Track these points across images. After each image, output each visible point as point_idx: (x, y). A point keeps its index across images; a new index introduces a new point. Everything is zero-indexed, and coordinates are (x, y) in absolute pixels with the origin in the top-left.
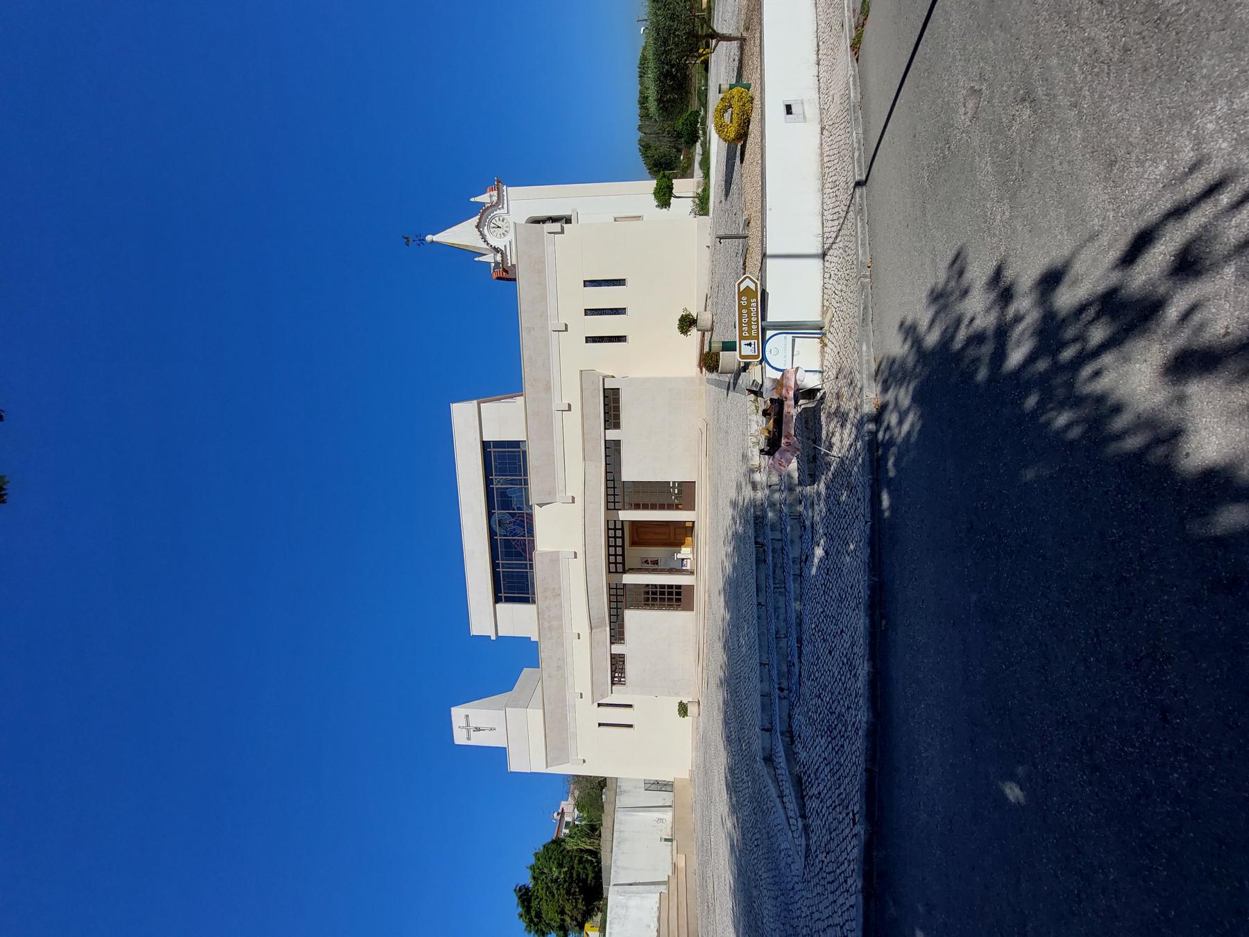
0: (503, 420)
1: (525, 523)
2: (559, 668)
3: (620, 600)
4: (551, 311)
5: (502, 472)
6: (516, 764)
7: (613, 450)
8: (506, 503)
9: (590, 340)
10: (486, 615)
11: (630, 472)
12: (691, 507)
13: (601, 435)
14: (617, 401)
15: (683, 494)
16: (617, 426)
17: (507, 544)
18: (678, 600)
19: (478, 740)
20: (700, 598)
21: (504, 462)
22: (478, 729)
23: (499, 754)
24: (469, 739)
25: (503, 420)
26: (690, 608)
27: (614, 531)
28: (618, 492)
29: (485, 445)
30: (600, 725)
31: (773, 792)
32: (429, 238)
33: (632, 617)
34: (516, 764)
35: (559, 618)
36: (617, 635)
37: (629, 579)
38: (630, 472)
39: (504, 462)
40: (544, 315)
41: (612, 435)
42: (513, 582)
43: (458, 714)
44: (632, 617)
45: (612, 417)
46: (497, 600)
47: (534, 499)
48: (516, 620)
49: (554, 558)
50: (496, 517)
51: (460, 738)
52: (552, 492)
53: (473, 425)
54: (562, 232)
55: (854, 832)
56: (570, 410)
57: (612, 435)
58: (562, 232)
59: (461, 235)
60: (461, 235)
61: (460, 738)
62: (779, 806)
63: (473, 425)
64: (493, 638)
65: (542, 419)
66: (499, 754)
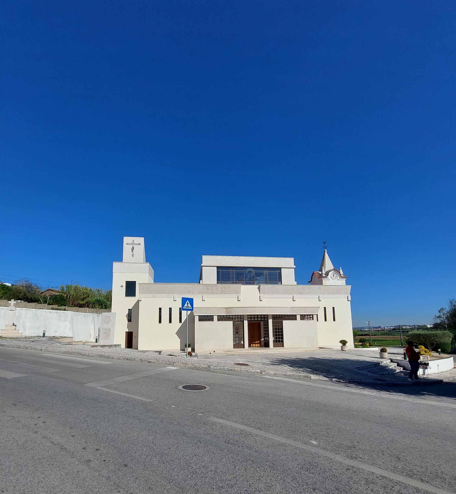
0: (288, 276)
1: (250, 281)
3: (237, 320)
4: (325, 296)
5: (270, 275)
6: (116, 265)
7: (293, 317)
8: (258, 275)
9: (170, 309)
10: (211, 263)
11: (286, 324)
12: (274, 346)
13: (298, 313)
14: (292, 319)
15: (279, 340)
16: (219, 320)
17: (242, 274)
18: (276, 341)
19: (126, 249)
20: (239, 351)
22: (133, 249)
23: (120, 259)
24: (127, 244)
25: (288, 276)
27: (265, 318)
28: (279, 319)
29: (280, 269)
31: (231, 376)
32: (326, 251)
33: (230, 324)
34: (116, 265)
35: (212, 293)
36: (221, 318)
38: (286, 324)
39: (274, 276)
40: (324, 293)
41: (215, 318)
42: (226, 275)
43: (141, 240)
44: (230, 324)
45: (303, 317)
46: (218, 268)
47: (262, 286)
48: (210, 275)
49: (238, 292)
50: (252, 270)
51: (127, 240)
52: (264, 293)
53: (286, 264)
54: (348, 301)
56: (260, 301)
57: (215, 318)
58: (348, 301)
59: (328, 265)
60: (328, 265)
61: (127, 240)
62: (234, 376)
63: (286, 264)
64: (202, 265)
66: (120, 259)
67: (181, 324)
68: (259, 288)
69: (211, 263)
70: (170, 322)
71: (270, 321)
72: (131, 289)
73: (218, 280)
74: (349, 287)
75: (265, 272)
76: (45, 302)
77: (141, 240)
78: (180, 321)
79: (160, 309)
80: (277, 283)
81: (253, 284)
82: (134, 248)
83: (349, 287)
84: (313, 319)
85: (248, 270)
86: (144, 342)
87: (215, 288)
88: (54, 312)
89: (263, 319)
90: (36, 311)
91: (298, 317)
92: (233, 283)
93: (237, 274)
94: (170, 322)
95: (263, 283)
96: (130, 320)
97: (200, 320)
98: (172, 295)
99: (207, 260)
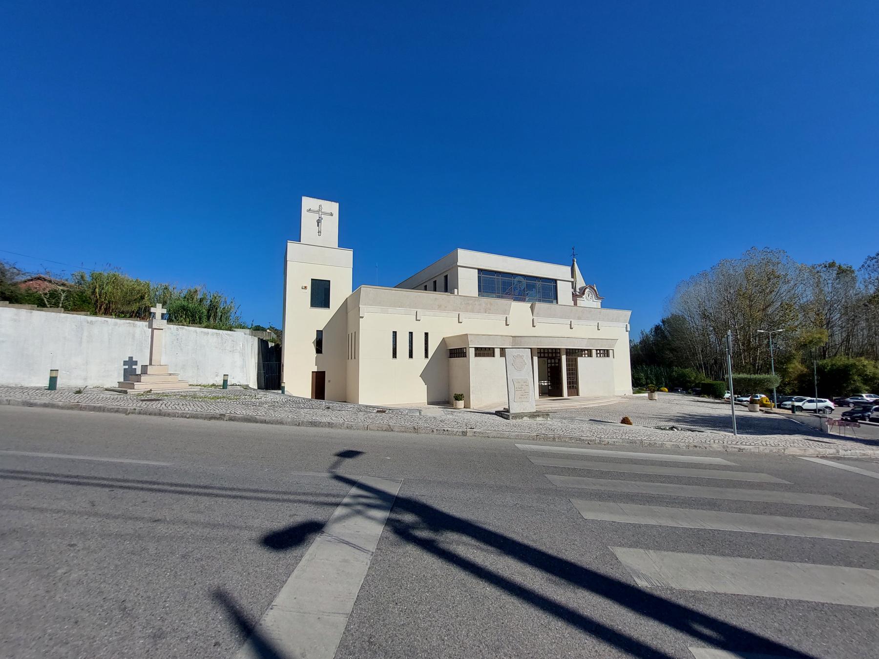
1: (520, 297)
2: (440, 306)
5: (544, 288)
6: (292, 246)
7: (589, 353)
8: (530, 287)
10: (470, 262)
14: (488, 355)
15: (574, 387)
17: (510, 284)
19: (308, 221)
21: (546, 290)
22: (319, 222)
23: (298, 239)
25: (564, 291)
26: (638, 384)
28: (573, 354)
29: (555, 281)
30: (426, 334)
34: (292, 246)
35: (472, 311)
37: (564, 358)
38: (582, 361)
39: (546, 290)
42: (494, 284)
43: (333, 207)
46: (480, 271)
47: (539, 305)
49: (506, 312)
50: (522, 279)
51: (308, 203)
52: (538, 315)
55: (47, 649)
56: (507, 325)
61: (308, 203)
65: (467, 304)
66: (298, 239)
67: (428, 360)
68: (532, 308)
69: (470, 262)
70: (411, 356)
71: (564, 358)
72: (320, 293)
73: (479, 291)
74: (348, 254)
75: (539, 284)
76: (56, 305)
77: (333, 207)
78: (426, 356)
79: (395, 333)
80: (552, 302)
81: (523, 300)
82: (320, 218)
83: (348, 254)
84: (608, 356)
85: (517, 279)
86: (369, 393)
87: (477, 303)
88: (213, 334)
89: (546, 355)
90: (177, 329)
91: (497, 352)
92: (499, 297)
93: (504, 283)
94: (411, 356)
95: (540, 301)
96: (319, 350)
97: (476, 355)
98: (414, 311)
99: (464, 256)
